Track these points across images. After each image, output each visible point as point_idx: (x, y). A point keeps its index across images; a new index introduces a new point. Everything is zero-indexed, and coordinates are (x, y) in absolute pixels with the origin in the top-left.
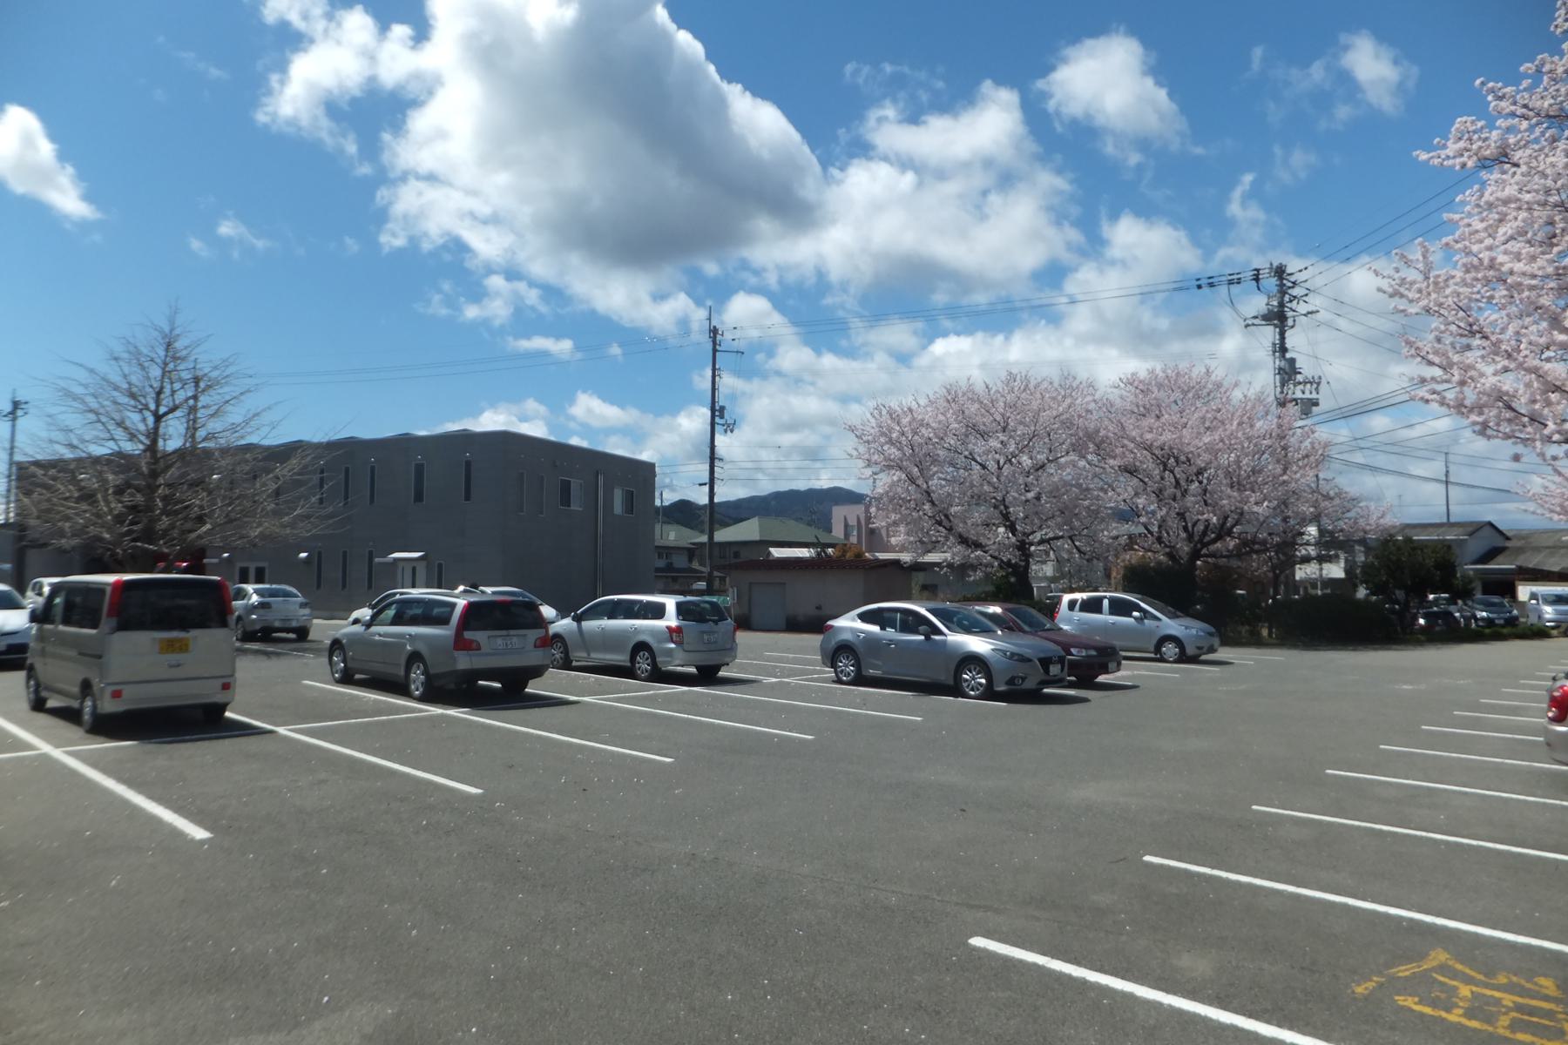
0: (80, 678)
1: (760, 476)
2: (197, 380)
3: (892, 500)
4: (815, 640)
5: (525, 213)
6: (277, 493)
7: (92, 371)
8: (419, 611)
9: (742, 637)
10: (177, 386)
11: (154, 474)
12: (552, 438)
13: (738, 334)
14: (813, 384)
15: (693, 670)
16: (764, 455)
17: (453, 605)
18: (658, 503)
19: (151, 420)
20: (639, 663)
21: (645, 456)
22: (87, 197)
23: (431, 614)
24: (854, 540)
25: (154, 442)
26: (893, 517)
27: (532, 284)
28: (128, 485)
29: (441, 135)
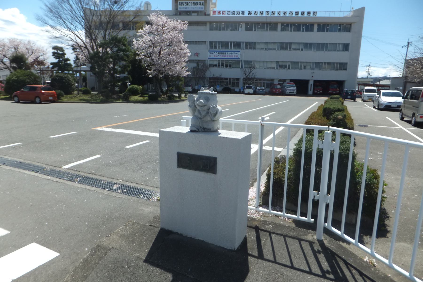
0: (412, 113)
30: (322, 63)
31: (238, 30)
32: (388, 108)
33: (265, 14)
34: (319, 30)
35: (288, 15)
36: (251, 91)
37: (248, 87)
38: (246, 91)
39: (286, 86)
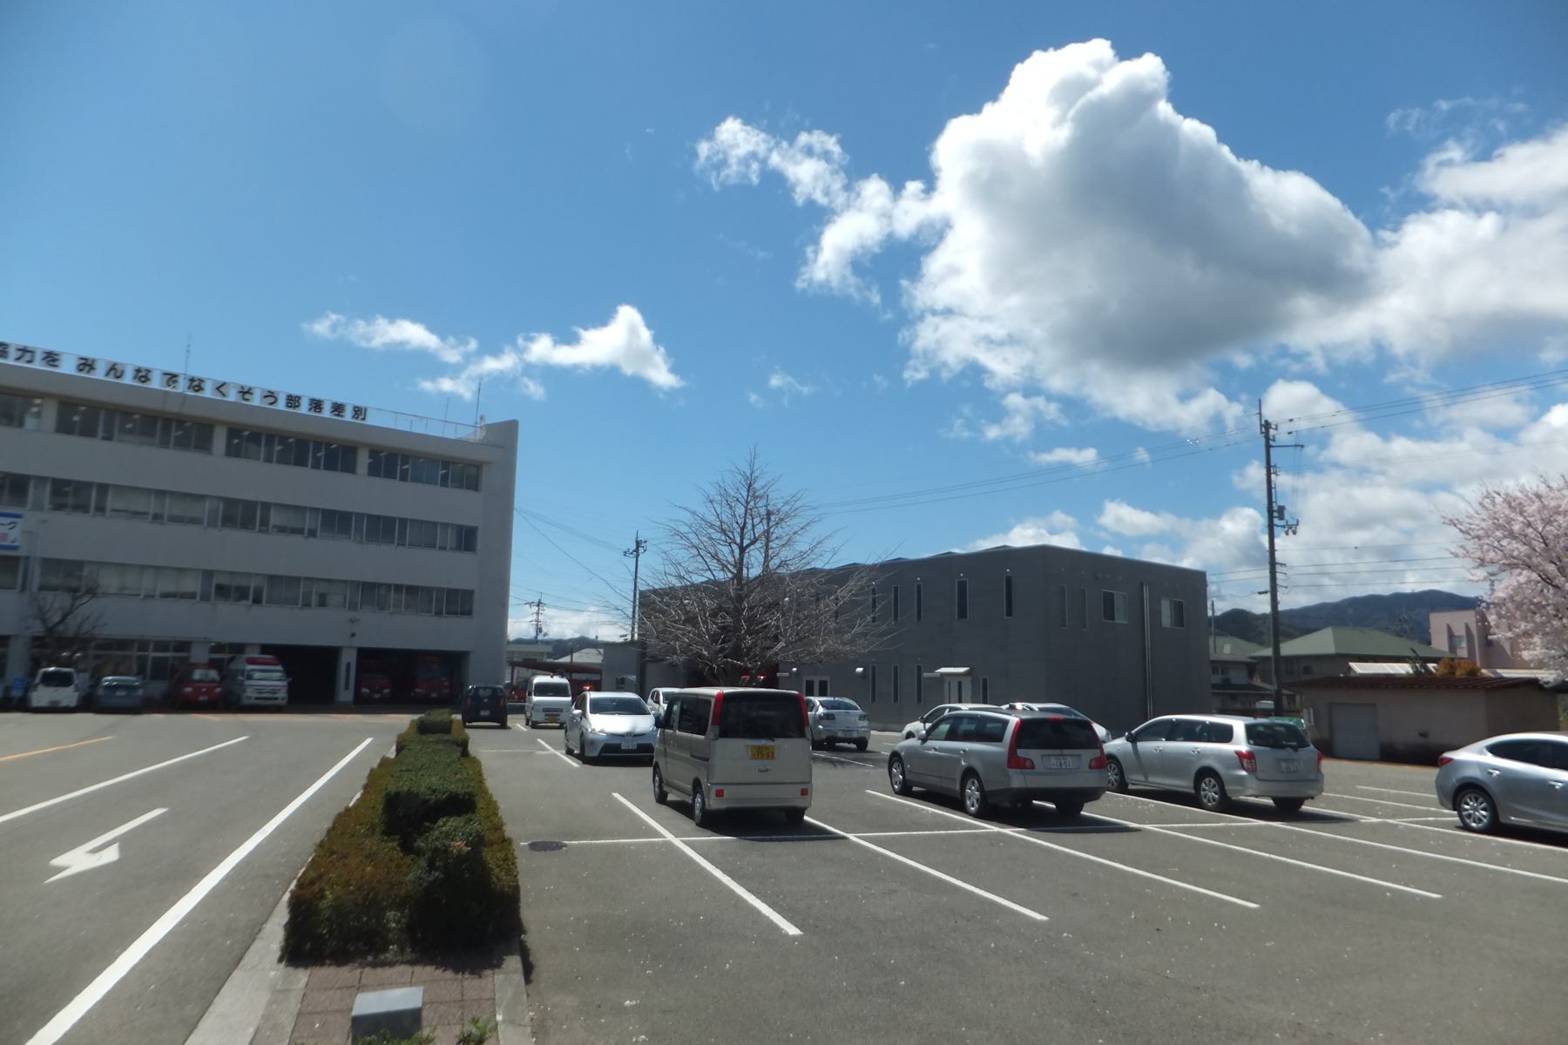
1: (1326, 581)
2: (769, 514)
3: (1521, 606)
4: (1430, 774)
5: (1038, 333)
6: (837, 614)
7: (694, 513)
8: (972, 727)
9: (1329, 766)
10: (757, 520)
11: (740, 599)
12: (1084, 549)
13: (1292, 427)
14: (1383, 473)
15: (1269, 802)
16: (1328, 557)
17: (1006, 723)
18: (1210, 613)
19: (737, 552)
20: (1204, 790)
21: (1187, 563)
22: (673, 370)
23: (986, 731)
24: (1463, 652)
25: (740, 571)
26: (1523, 626)
27: (1050, 398)
28: (720, 608)
29: (954, 271)
30: (389, 586)
31: (21, 424)
32: (613, 754)
33: (156, 383)
34: (374, 471)
35: (256, 400)
36: (68, 695)
37: (50, 680)
38: (42, 696)
39: (242, 672)
